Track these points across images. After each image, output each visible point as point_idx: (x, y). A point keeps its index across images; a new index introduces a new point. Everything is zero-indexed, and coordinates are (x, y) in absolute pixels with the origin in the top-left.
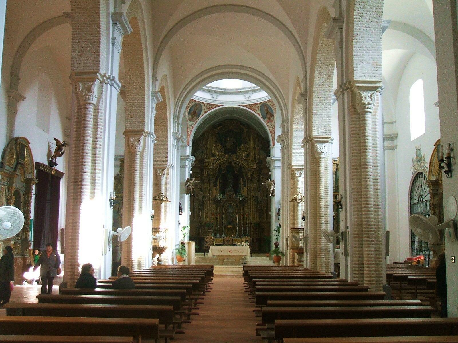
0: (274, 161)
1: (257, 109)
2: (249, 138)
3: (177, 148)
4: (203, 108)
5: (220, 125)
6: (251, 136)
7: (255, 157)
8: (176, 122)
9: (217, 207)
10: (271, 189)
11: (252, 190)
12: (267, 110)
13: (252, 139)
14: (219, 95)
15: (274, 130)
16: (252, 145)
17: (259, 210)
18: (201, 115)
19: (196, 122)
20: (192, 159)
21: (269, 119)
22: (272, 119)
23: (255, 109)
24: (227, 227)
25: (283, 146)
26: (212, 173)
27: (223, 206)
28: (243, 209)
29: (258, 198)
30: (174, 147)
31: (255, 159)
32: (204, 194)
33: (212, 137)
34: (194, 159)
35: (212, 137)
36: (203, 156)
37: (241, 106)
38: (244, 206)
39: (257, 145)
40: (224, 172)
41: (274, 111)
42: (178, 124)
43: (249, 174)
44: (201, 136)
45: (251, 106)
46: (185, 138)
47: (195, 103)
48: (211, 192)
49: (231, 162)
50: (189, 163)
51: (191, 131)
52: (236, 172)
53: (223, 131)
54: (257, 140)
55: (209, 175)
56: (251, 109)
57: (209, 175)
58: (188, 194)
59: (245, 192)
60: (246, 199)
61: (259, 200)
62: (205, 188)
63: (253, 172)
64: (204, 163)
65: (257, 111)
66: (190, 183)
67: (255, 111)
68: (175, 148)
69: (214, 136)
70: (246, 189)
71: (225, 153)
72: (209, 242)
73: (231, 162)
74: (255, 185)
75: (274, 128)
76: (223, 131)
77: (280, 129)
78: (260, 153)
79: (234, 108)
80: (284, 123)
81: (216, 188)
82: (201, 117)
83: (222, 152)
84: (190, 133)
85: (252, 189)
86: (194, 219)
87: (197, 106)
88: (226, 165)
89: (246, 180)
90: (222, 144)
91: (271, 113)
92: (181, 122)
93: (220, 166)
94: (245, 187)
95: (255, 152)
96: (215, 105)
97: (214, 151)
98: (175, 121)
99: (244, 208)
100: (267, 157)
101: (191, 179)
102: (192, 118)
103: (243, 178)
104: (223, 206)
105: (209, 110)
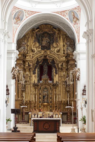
0: (79, 54)
1: (66, 15)
2: (60, 37)
3: (4, 41)
4: (25, 14)
5: (37, 28)
6: (61, 37)
7: (64, 52)
8: (3, 21)
9: (36, 89)
10: (77, 75)
11: (62, 77)
12: (74, 15)
13: (61, 38)
14: (37, 4)
15: (79, 31)
16: (61, 44)
17: (67, 91)
18: (23, 20)
19: (19, 25)
20: (16, 53)
21: (75, 22)
22: (77, 22)
23: (65, 15)
24: (43, 104)
25: (88, 40)
26: (31, 64)
27: (40, 89)
28: (55, 91)
29: (66, 83)
30: (2, 40)
31: (64, 53)
32: (26, 80)
33: (32, 38)
34: (18, 53)
35: (32, 38)
36: (25, 51)
37: (54, 12)
38: (56, 88)
39: (66, 43)
40: (41, 63)
41: (79, 16)
42: (5, 23)
43: (60, 65)
44: (24, 36)
45: (61, 13)
46: (10, 34)
47: (18, 10)
48: (31, 78)
49: (46, 56)
50: (14, 56)
51: (16, 31)
52: (50, 63)
53: (40, 33)
54: (65, 39)
55: (29, 66)
56: (61, 15)
57: (29, 66)
58: (14, 79)
59: (56, 78)
60: (58, 83)
61: (67, 84)
62: (27, 75)
63: (63, 63)
64: (25, 57)
65: (66, 16)
66: (15, 70)
67: (65, 16)
68: (3, 42)
69: (33, 37)
70: (57, 76)
71: (42, 49)
72: (46, 116)
73: (46, 56)
74: (64, 73)
75: (79, 29)
76: (40, 33)
77: (85, 27)
78: (68, 49)
79: (48, 14)
80: (89, 21)
81: (35, 75)
82: (23, 21)
83: (39, 48)
84: (15, 33)
85: (62, 76)
86: (18, 98)
87: (20, 13)
88: (43, 58)
89: (58, 70)
90: (39, 43)
91: (77, 17)
92: (7, 21)
93: (38, 59)
94: (57, 74)
95: (64, 49)
96: (33, 12)
97: (33, 48)
98: (2, 21)
99: (56, 90)
100: (73, 51)
101: (16, 68)
102: (17, 22)
103: (55, 68)
104: (40, 89)
105: (29, 16)
